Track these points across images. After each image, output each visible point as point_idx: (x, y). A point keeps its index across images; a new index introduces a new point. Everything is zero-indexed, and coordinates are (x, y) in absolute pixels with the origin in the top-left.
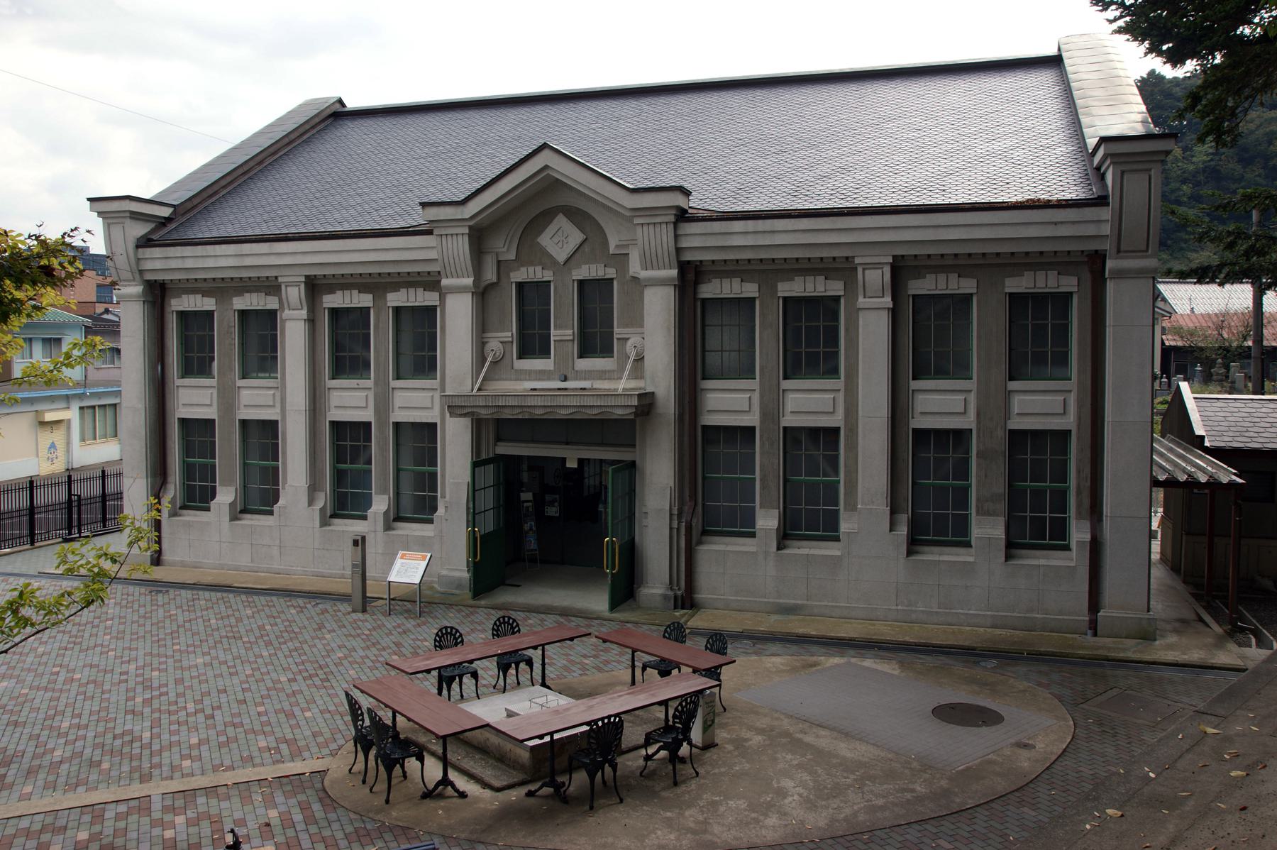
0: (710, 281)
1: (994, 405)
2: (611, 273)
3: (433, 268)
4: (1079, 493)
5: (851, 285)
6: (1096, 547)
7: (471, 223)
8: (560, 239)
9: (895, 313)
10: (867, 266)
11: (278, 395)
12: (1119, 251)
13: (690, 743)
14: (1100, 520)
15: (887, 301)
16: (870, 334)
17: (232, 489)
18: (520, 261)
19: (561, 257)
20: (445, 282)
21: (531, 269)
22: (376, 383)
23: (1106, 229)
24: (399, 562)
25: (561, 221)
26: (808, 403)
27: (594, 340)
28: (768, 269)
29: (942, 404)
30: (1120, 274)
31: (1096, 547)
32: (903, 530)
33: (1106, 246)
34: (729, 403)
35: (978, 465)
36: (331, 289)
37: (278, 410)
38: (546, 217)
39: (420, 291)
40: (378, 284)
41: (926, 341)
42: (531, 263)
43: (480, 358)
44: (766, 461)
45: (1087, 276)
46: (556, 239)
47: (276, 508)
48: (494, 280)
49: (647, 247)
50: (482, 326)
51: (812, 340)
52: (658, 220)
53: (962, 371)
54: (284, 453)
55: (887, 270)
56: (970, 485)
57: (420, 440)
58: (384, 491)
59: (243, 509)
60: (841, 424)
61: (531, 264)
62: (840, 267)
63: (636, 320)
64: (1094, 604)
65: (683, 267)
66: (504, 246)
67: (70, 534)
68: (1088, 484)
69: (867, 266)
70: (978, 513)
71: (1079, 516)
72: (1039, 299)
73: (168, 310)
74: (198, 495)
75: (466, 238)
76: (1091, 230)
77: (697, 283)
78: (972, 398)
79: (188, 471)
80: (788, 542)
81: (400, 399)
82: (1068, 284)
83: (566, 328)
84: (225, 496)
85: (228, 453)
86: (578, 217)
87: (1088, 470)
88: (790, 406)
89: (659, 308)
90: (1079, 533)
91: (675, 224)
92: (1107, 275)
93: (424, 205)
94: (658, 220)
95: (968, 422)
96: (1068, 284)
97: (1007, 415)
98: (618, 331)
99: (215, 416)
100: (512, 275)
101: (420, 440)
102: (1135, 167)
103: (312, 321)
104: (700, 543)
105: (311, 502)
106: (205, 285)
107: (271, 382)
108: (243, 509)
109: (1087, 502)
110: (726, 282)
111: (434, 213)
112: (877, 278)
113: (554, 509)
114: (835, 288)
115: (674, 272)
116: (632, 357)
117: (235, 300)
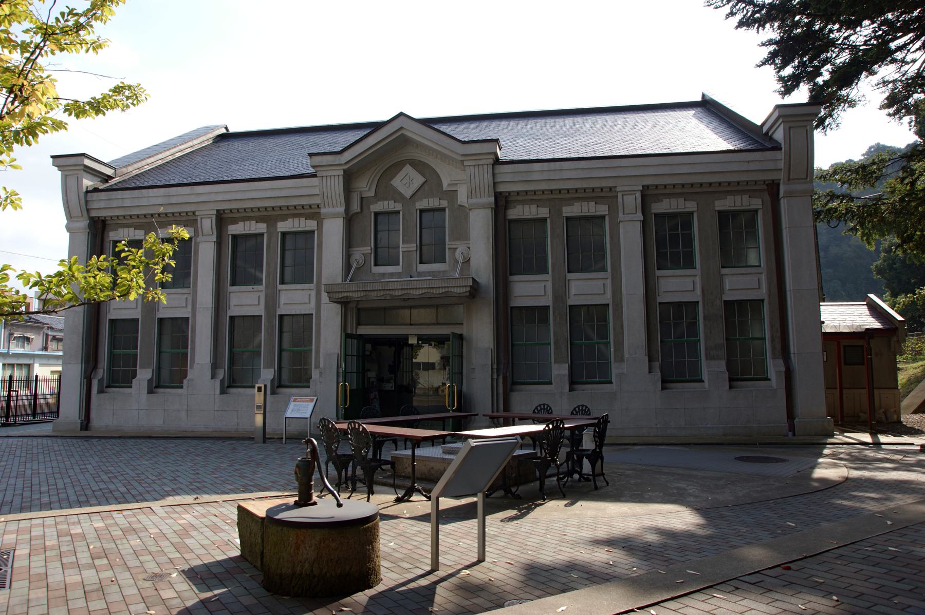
0: (515, 207)
1: (712, 285)
2: (444, 203)
3: (317, 201)
4: (773, 340)
5: (613, 210)
6: (788, 375)
7: (345, 167)
8: (407, 181)
9: (644, 223)
10: (625, 193)
11: (190, 299)
12: (789, 180)
13: (580, 473)
14: (789, 358)
15: (640, 216)
16: (629, 239)
17: (151, 370)
18: (377, 197)
19: (408, 193)
20: (323, 211)
21: (386, 203)
22: (267, 287)
23: (781, 165)
24: (292, 405)
25: (408, 169)
26: (585, 289)
27: (432, 250)
28: (555, 197)
29: (678, 285)
30: (789, 195)
31: (788, 375)
32: (658, 375)
33: (782, 176)
34: (530, 290)
35: (705, 325)
36: (284, 218)
37: (190, 308)
38: (397, 167)
39: (303, 220)
40: (270, 215)
41: (668, 242)
42: (385, 199)
43: (348, 266)
44: (556, 331)
45: (767, 198)
46: (404, 181)
47: (185, 381)
48: (359, 210)
49: (473, 182)
50: (349, 243)
51: (586, 247)
52: (481, 162)
53: (689, 263)
54: (193, 342)
55: (639, 195)
56: (699, 340)
57: (298, 330)
58: (269, 366)
59: (154, 386)
60: (610, 302)
61: (385, 199)
62: (607, 195)
63: (462, 234)
64: (791, 415)
65: (498, 196)
66: (365, 186)
67: (7, 420)
68: (779, 334)
69: (625, 193)
70: (707, 358)
71: (774, 357)
72: (735, 214)
73: (107, 240)
74: (120, 377)
75: (341, 178)
76: (771, 166)
77: (506, 208)
78: (698, 280)
79: (113, 359)
80: (576, 386)
81: (284, 298)
82: (756, 203)
83: (411, 242)
84: (144, 375)
85: (146, 343)
86: (419, 166)
87: (778, 325)
88: (573, 291)
89: (480, 224)
90: (774, 368)
91: (493, 165)
92: (781, 194)
93: (311, 155)
94: (481, 162)
95: (697, 296)
96: (756, 203)
97: (722, 292)
98: (449, 244)
99: (139, 317)
100: (371, 207)
101: (298, 330)
102: (797, 124)
103: (219, 244)
104: (512, 390)
105: (213, 376)
106: (137, 221)
107: (185, 290)
108: (154, 386)
109: (778, 346)
110: (526, 208)
111: (318, 160)
112: (632, 202)
113: (390, 385)
114: (311, 225)
115: (492, 199)
116: (461, 260)
117: (717, 203)
